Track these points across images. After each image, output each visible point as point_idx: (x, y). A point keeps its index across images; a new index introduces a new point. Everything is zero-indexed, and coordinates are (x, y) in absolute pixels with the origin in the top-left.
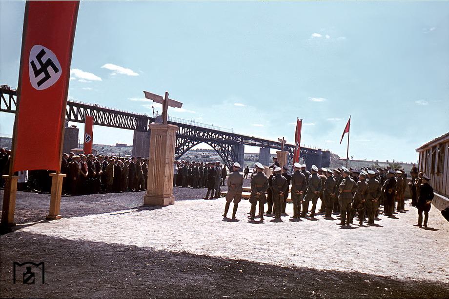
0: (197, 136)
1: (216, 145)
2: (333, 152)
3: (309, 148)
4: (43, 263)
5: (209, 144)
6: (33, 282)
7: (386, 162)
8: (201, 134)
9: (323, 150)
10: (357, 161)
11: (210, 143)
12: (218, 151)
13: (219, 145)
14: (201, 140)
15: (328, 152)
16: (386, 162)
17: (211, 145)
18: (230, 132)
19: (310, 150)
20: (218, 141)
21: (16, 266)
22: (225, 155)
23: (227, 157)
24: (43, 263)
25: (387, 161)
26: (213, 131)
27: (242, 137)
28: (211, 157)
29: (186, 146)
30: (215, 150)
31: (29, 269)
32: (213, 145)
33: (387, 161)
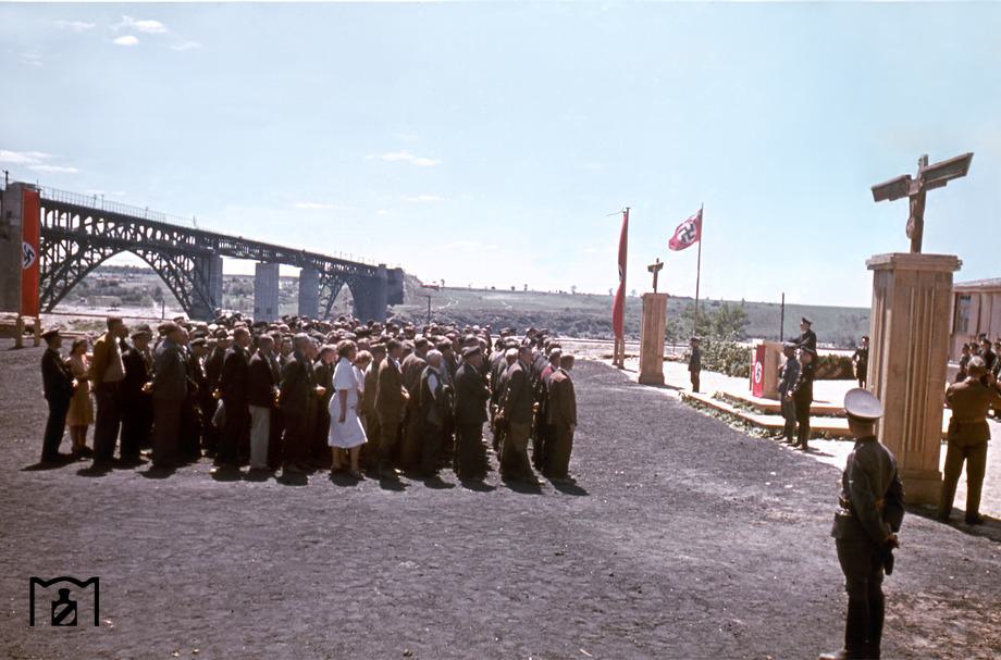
0: (175, 243)
1: (155, 257)
2: (408, 270)
3: (361, 262)
4: (95, 580)
5: (139, 255)
6: (74, 623)
7: (510, 289)
8: (101, 227)
9: (388, 267)
10: (453, 289)
11: (141, 252)
12: (160, 272)
13: (162, 257)
14: (119, 245)
15: (399, 270)
16: (510, 289)
17: (144, 257)
18: (189, 224)
19: (362, 267)
20: (167, 251)
21: (37, 585)
22: (178, 280)
23: (182, 285)
24: (95, 580)
25: (513, 288)
26: (147, 224)
27: (216, 238)
28: (122, 286)
29: (87, 259)
30: (155, 268)
31: (64, 593)
32: (149, 257)
33: (513, 288)
